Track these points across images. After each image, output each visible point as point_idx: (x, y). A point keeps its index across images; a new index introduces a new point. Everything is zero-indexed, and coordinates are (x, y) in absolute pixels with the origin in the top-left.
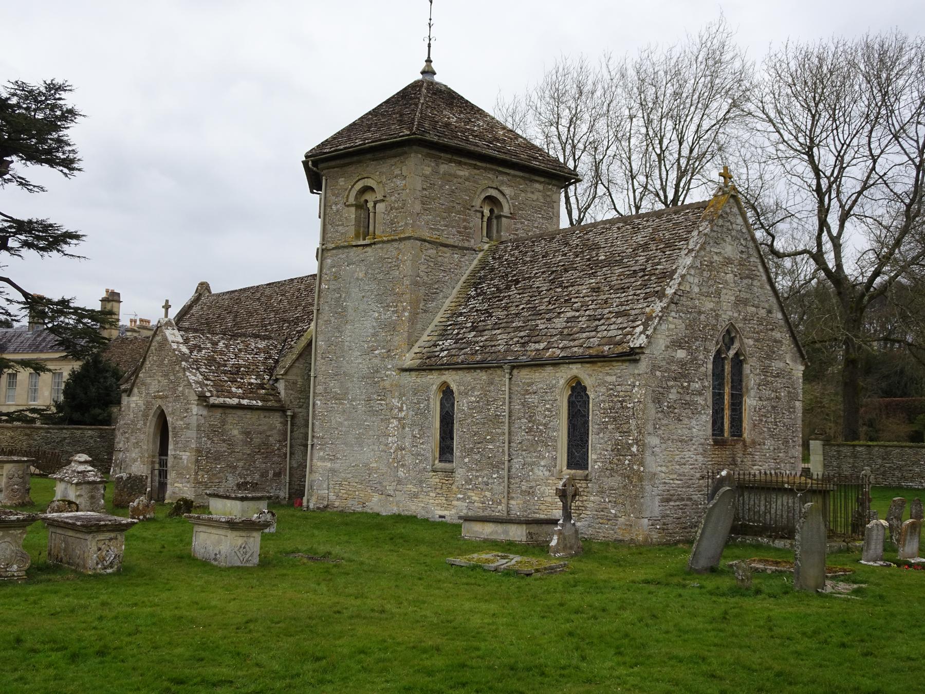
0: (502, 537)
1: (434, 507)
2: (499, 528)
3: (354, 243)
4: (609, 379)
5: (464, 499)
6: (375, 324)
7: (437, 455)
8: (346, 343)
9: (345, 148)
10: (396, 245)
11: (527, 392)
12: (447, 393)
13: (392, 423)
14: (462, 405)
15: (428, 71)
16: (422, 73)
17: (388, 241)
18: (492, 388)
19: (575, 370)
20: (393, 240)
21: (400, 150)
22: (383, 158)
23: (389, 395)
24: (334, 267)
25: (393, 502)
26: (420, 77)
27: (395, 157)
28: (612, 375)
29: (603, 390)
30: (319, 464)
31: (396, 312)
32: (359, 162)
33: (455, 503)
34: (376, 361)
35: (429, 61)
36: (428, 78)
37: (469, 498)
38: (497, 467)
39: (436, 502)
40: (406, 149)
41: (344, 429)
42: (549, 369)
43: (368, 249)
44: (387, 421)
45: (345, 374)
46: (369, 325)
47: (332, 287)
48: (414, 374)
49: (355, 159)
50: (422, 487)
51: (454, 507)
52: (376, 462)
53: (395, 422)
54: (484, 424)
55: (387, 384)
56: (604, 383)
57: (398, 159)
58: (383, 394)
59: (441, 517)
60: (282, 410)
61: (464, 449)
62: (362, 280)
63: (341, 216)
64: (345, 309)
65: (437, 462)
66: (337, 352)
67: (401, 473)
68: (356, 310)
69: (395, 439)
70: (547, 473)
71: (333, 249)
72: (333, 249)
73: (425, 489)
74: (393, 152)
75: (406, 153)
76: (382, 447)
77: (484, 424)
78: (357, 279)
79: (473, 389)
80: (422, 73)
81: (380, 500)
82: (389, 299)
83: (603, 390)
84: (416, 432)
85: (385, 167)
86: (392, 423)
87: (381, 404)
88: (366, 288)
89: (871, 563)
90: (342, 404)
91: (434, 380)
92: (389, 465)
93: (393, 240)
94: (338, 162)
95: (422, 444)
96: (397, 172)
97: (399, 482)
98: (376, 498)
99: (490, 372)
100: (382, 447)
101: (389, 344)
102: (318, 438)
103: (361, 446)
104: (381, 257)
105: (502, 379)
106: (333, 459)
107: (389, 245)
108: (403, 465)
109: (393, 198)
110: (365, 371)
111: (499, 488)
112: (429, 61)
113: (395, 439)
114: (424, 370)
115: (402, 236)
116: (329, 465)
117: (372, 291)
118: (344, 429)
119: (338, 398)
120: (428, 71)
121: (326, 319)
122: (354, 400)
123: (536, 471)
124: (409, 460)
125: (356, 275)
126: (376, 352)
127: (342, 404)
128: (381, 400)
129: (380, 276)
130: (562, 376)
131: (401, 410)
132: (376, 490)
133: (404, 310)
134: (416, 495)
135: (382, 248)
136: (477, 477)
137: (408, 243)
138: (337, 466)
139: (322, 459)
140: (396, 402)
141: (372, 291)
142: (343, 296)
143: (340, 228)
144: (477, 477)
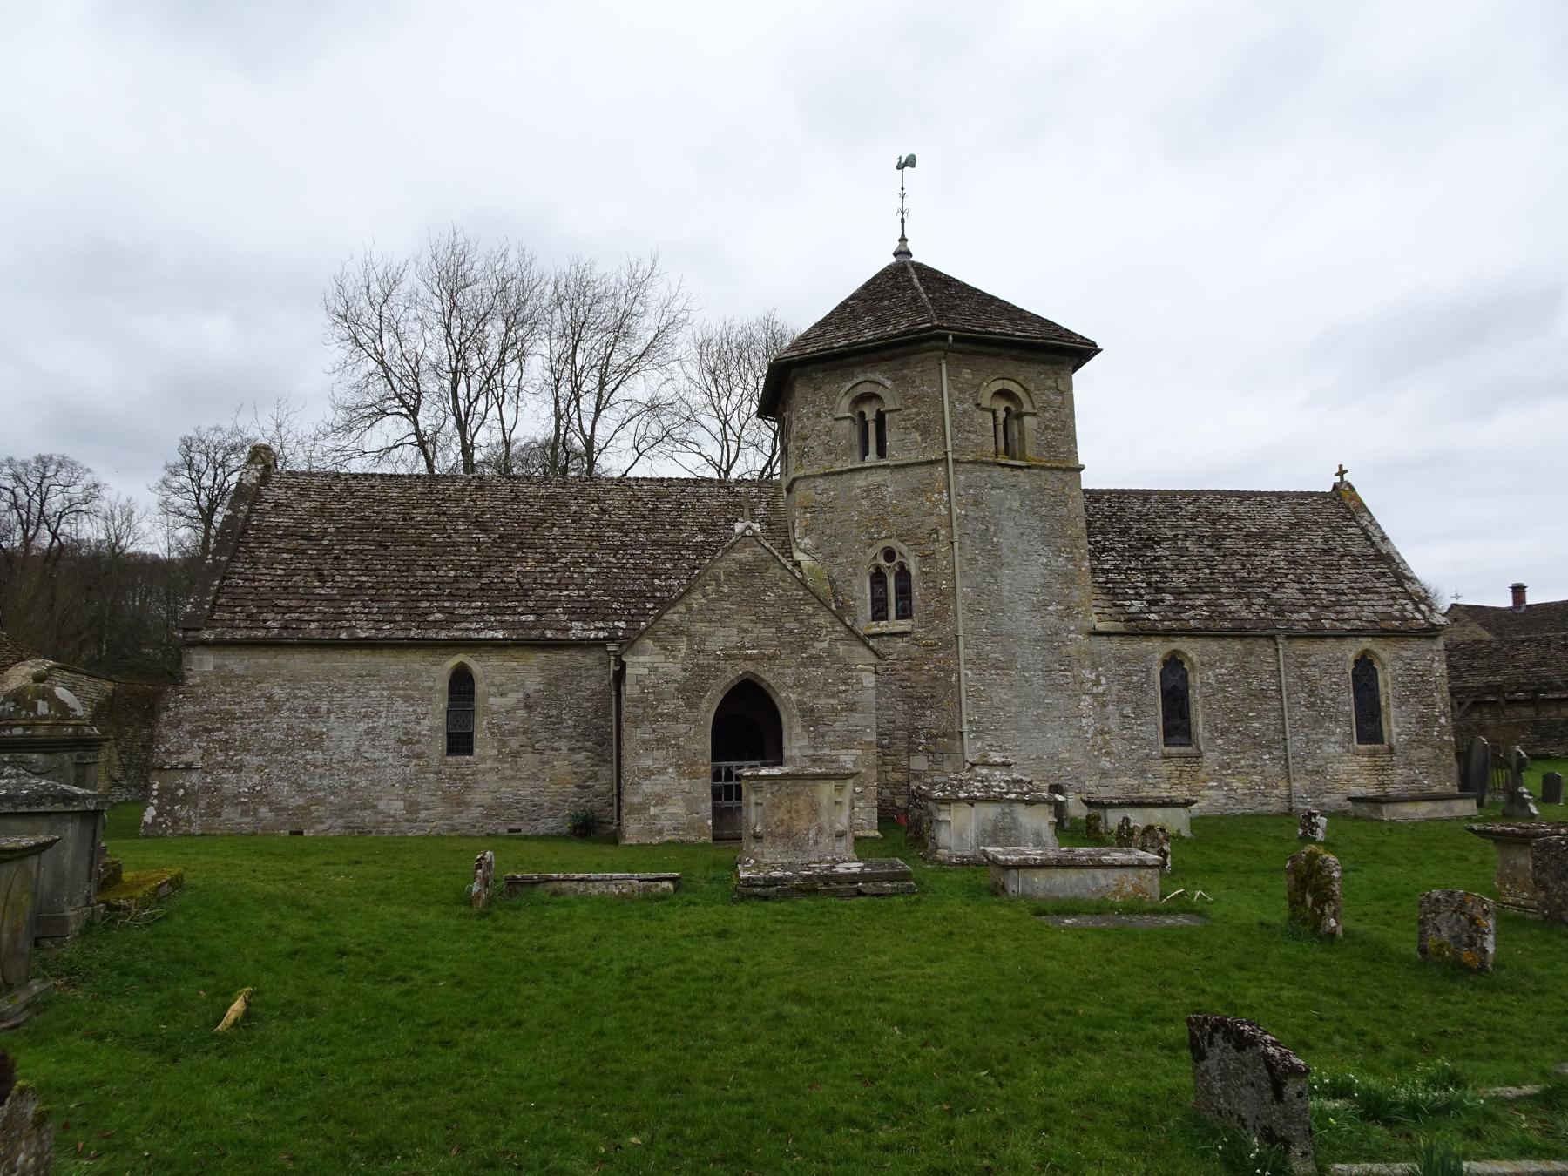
0: (1445, 815)
2: (1440, 806)
4: (1405, 653)
5: (1220, 787)
10: (1059, 474)
11: (1303, 665)
14: (1199, 682)
15: (902, 253)
16: (895, 255)
17: (1052, 468)
18: (1252, 659)
19: (1366, 643)
20: (1057, 468)
23: (1076, 665)
26: (893, 260)
28: (1409, 649)
29: (1400, 664)
32: (997, 355)
34: (1053, 620)
35: (903, 239)
36: (903, 259)
37: (1227, 784)
38: (1268, 747)
42: (1331, 641)
44: (1076, 698)
45: (1010, 635)
48: (1116, 639)
49: (995, 350)
53: (1089, 700)
55: (1072, 650)
56: (1399, 657)
58: (1068, 663)
62: (1017, 511)
64: (996, 547)
67: (1105, 763)
70: (1340, 750)
71: (969, 462)
72: (969, 462)
74: (1049, 357)
76: (1074, 732)
78: (1010, 509)
79: (1223, 659)
80: (895, 255)
82: (1060, 542)
83: (1400, 664)
91: (1157, 650)
92: (1086, 754)
93: (1057, 468)
94: (969, 347)
96: (1050, 383)
97: (1104, 774)
100: (1074, 732)
103: (1041, 730)
105: (1262, 648)
107: (1047, 473)
108: (1107, 754)
110: (1039, 633)
111: (1274, 770)
112: (903, 239)
119: (1002, 668)
120: (902, 253)
122: (1024, 669)
123: (1325, 747)
124: (1118, 746)
129: (1043, 511)
130: (1351, 650)
131: (1097, 683)
135: (1039, 475)
136: (1238, 760)
140: (1086, 673)
143: (973, 436)
144: (1238, 760)
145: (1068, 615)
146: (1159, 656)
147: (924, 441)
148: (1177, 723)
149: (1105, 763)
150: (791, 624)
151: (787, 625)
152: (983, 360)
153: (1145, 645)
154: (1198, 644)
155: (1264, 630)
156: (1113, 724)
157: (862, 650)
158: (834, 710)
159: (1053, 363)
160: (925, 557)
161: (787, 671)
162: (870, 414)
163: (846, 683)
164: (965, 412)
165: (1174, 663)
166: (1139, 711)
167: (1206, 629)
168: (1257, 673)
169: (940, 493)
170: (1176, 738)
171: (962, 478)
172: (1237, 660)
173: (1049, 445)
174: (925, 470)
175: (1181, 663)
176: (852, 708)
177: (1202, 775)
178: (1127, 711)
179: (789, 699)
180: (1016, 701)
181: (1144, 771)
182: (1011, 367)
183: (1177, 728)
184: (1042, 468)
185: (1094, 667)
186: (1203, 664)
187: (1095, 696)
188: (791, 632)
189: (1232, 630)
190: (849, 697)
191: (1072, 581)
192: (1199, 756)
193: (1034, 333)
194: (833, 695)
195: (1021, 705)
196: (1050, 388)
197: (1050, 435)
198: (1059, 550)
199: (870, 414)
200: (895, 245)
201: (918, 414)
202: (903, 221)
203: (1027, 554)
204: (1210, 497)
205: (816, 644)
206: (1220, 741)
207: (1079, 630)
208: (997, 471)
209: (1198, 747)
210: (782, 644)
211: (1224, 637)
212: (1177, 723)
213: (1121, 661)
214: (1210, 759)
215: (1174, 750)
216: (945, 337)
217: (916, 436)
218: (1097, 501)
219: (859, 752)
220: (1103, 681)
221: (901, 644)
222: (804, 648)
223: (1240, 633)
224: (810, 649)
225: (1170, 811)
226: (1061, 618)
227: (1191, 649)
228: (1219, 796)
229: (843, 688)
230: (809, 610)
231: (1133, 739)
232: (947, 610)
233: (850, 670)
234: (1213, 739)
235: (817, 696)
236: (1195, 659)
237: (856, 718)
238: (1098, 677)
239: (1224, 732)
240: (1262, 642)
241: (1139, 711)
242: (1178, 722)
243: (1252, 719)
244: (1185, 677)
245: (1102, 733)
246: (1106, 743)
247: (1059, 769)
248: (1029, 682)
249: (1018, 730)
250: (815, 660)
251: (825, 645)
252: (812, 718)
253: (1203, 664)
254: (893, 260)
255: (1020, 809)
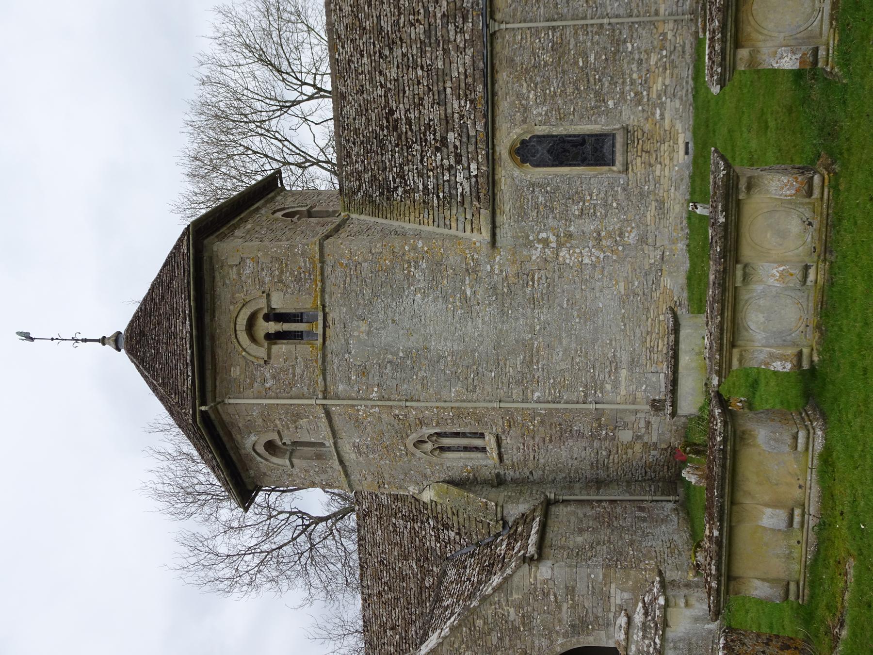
1: (675, 162)
3: (320, 340)
5: (662, 106)
6: (431, 298)
7: (606, 168)
8: (455, 347)
9: (191, 347)
10: (328, 270)
12: (525, 152)
13: (564, 257)
14: (545, 124)
15: (116, 341)
17: (323, 281)
18: (518, 59)
21: (206, 266)
22: (213, 298)
23: (527, 266)
24: (349, 378)
25: (671, 250)
27: (214, 277)
30: (623, 392)
31: (416, 262)
32: (213, 338)
33: (667, 124)
35: (103, 341)
36: (122, 342)
37: (659, 97)
38: (619, 43)
39: (667, 162)
40: (206, 255)
41: (573, 345)
43: (330, 319)
45: (497, 346)
46: (431, 309)
47: (377, 380)
48: (499, 219)
49: (208, 343)
50: (649, 192)
51: (673, 126)
52: (617, 283)
53: (563, 253)
54: (564, 72)
55: (511, 270)
57: (217, 274)
58: (526, 276)
59: (687, 153)
60: (548, 504)
61: (597, 110)
63: (282, 370)
64: (408, 353)
65: (614, 168)
66: (465, 363)
67: (631, 238)
68: (410, 333)
69: (585, 251)
71: (325, 379)
72: (325, 379)
73: (652, 187)
74: (207, 277)
75: (211, 258)
76: (597, 275)
77: (564, 72)
78: (369, 333)
79: (519, 96)
80: (119, 350)
81: (670, 273)
82: (399, 276)
84: (575, 209)
85: (224, 294)
86: (564, 257)
87: (540, 278)
88: (381, 317)
89: (707, 57)
90: (538, 352)
91: (510, 174)
93: (322, 268)
94: (208, 373)
95: (591, 195)
96: (233, 273)
97: (643, 240)
98: (667, 282)
99: (497, 66)
101: (458, 270)
102: (585, 396)
104: (343, 294)
105: (504, 49)
106: (615, 364)
107: (328, 283)
108: (621, 235)
109: (267, 279)
110: (493, 310)
112: (103, 341)
113: (585, 251)
114: (494, 195)
115: (317, 257)
116: (624, 373)
117: (388, 306)
118: (573, 345)
120: (116, 341)
121: (419, 387)
122: (532, 330)
124: (613, 223)
125: (364, 336)
126: (468, 293)
127: (538, 348)
128: (533, 280)
129: (368, 292)
132: (657, 282)
133: (414, 248)
134: (661, 203)
135: (332, 294)
136: (633, 82)
137: (327, 250)
138: (625, 357)
139: (616, 386)
140: (536, 254)
141: (388, 306)
142: (390, 356)
143: (298, 370)
144: (633, 82)
145: (476, 272)
146: (517, 173)
147: (307, 417)
148: (587, 150)
149: (631, 238)
150: (494, 638)
151: (495, 641)
152: (220, 352)
153: (504, 186)
154: (503, 126)
155: (485, 46)
156: (590, 226)
157: (516, 579)
158: (574, 607)
159: (212, 270)
160: (422, 423)
161: (537, 643)
162: (273, 327)
163: (548, 593)
164: (274, 377)
165: (525, 152)
166: (576, 197)
167: (485, 116)
168: (534, 53)
169: (358, 410)
170: (606, 149)
171: (341, 387)
172: (519, 79)
173: (298, 279)
174: (336, 419)
175: (523, 142)
176: (571, 591)
177: (647, 127)
178: (575, 209)
179: (562, 645)
180: (565, 342)
181: (641, 194)
182: (223, 319)
183: (595, 150)
184: (323, 290)
185: (529, 245)
186: (524, 121)
187: (560, 245)
188: (500, 639)
189: (486, 85)
190: (561, 592)
191: (439, 264)
192: (626, 130)
193: (183, 281)
194: (559, 607)
195: (570, 336)
196: (239, 274)
197: (287, 277)
198: (407, 277)
199: (273, 327)
200: (109, 349)
201: (281, 420)
202: (85, 340)
203: (413, 317)
204: (334, 18)
205: (512, 618)
206: (611, 103)
207: (491, 259)
208: (331, 345)
209: (618, 129)
210: (512, 647)
211: (494, 94)
212: (587, 150)
213: (523, 214)
214: (630, 116)
215: (619, 158)
216: (203, 403)
217: (303, 422)
218: (349, 155)
219: (613, 586)
220: (543, 235)
221: (507, 441)
222: (516, 629)
223: (489, 76)
224: (516, 624)
225: (682, 346)
226: (478, 281)
227: (508, 135)
228: (672, 106)
229: (552, 598)
230: (479, 623)
231: (606, 205)
232: (474, 413)
233: (536, 588)
234: (608, 111)
235: (560, 621)
236: (518, 130)
237: (581, 587)
238: (540, 241)
239: (601, 98)
240: (498, 48)
241: (576, 197)
242: (588, 148)
243: (586, 62)
244: (540, 138)
245: (599, 239)
246: (610, 235)
247: (636, 294)
248: (545, 325)
249: (594, 342)
250: (526, 620)
251: (512, 610)
252: (580, 626)
253: (524, 121)
254: (123, 351)
255: (671, 634)
